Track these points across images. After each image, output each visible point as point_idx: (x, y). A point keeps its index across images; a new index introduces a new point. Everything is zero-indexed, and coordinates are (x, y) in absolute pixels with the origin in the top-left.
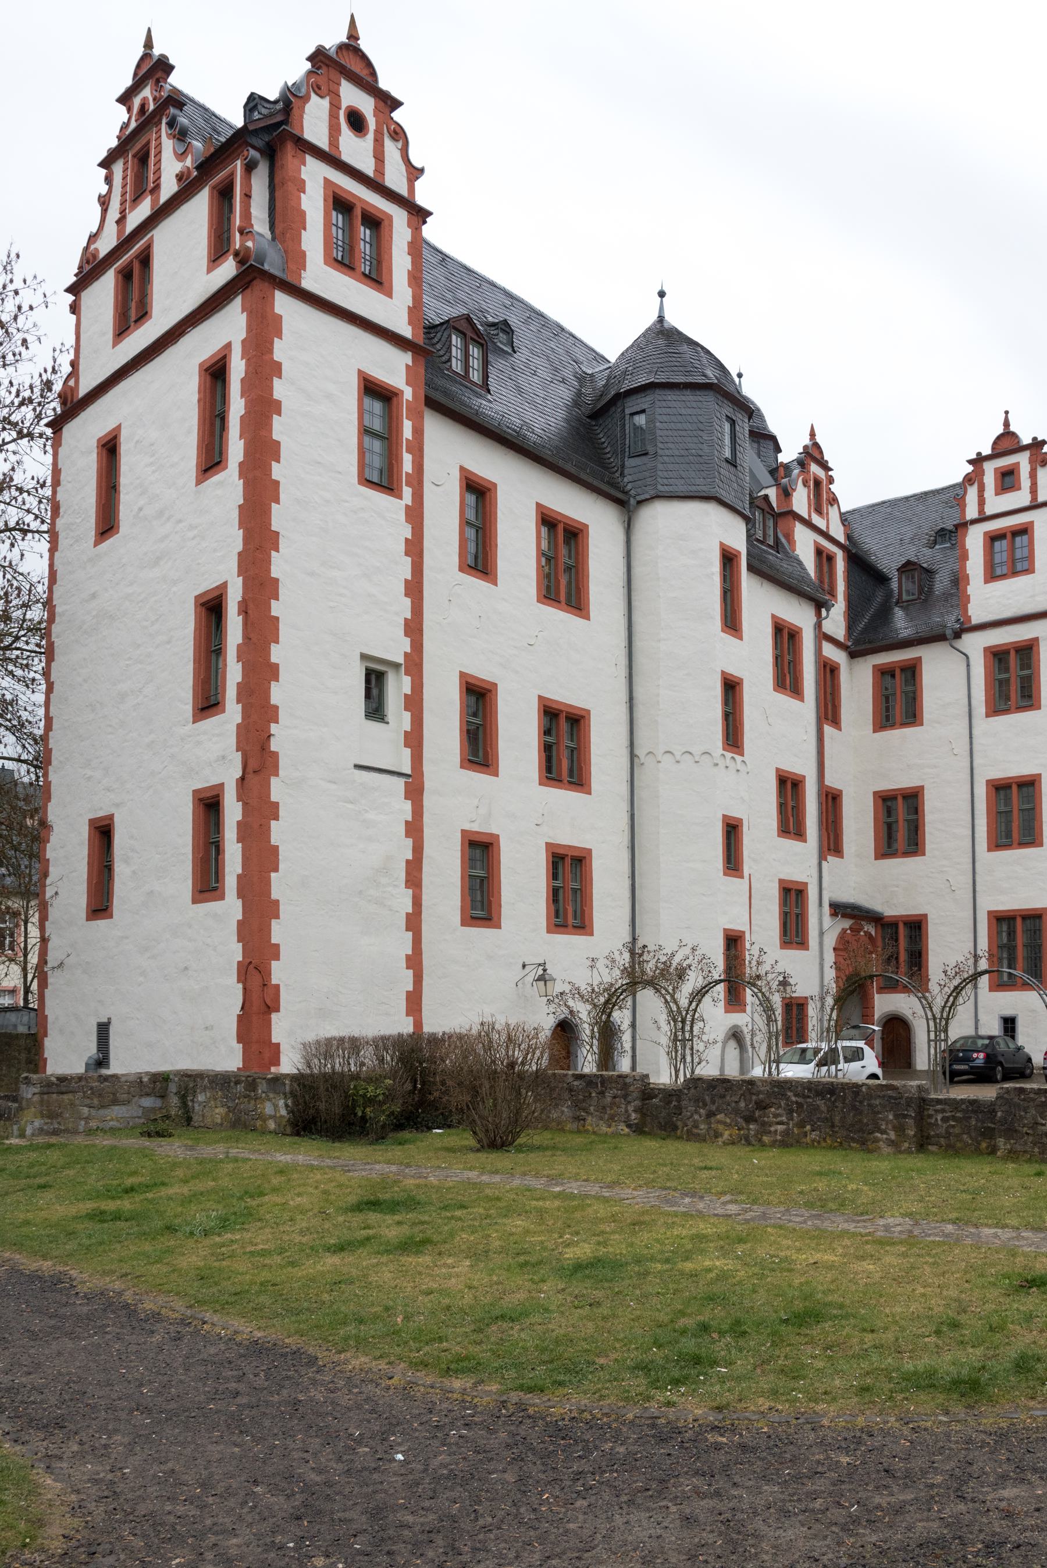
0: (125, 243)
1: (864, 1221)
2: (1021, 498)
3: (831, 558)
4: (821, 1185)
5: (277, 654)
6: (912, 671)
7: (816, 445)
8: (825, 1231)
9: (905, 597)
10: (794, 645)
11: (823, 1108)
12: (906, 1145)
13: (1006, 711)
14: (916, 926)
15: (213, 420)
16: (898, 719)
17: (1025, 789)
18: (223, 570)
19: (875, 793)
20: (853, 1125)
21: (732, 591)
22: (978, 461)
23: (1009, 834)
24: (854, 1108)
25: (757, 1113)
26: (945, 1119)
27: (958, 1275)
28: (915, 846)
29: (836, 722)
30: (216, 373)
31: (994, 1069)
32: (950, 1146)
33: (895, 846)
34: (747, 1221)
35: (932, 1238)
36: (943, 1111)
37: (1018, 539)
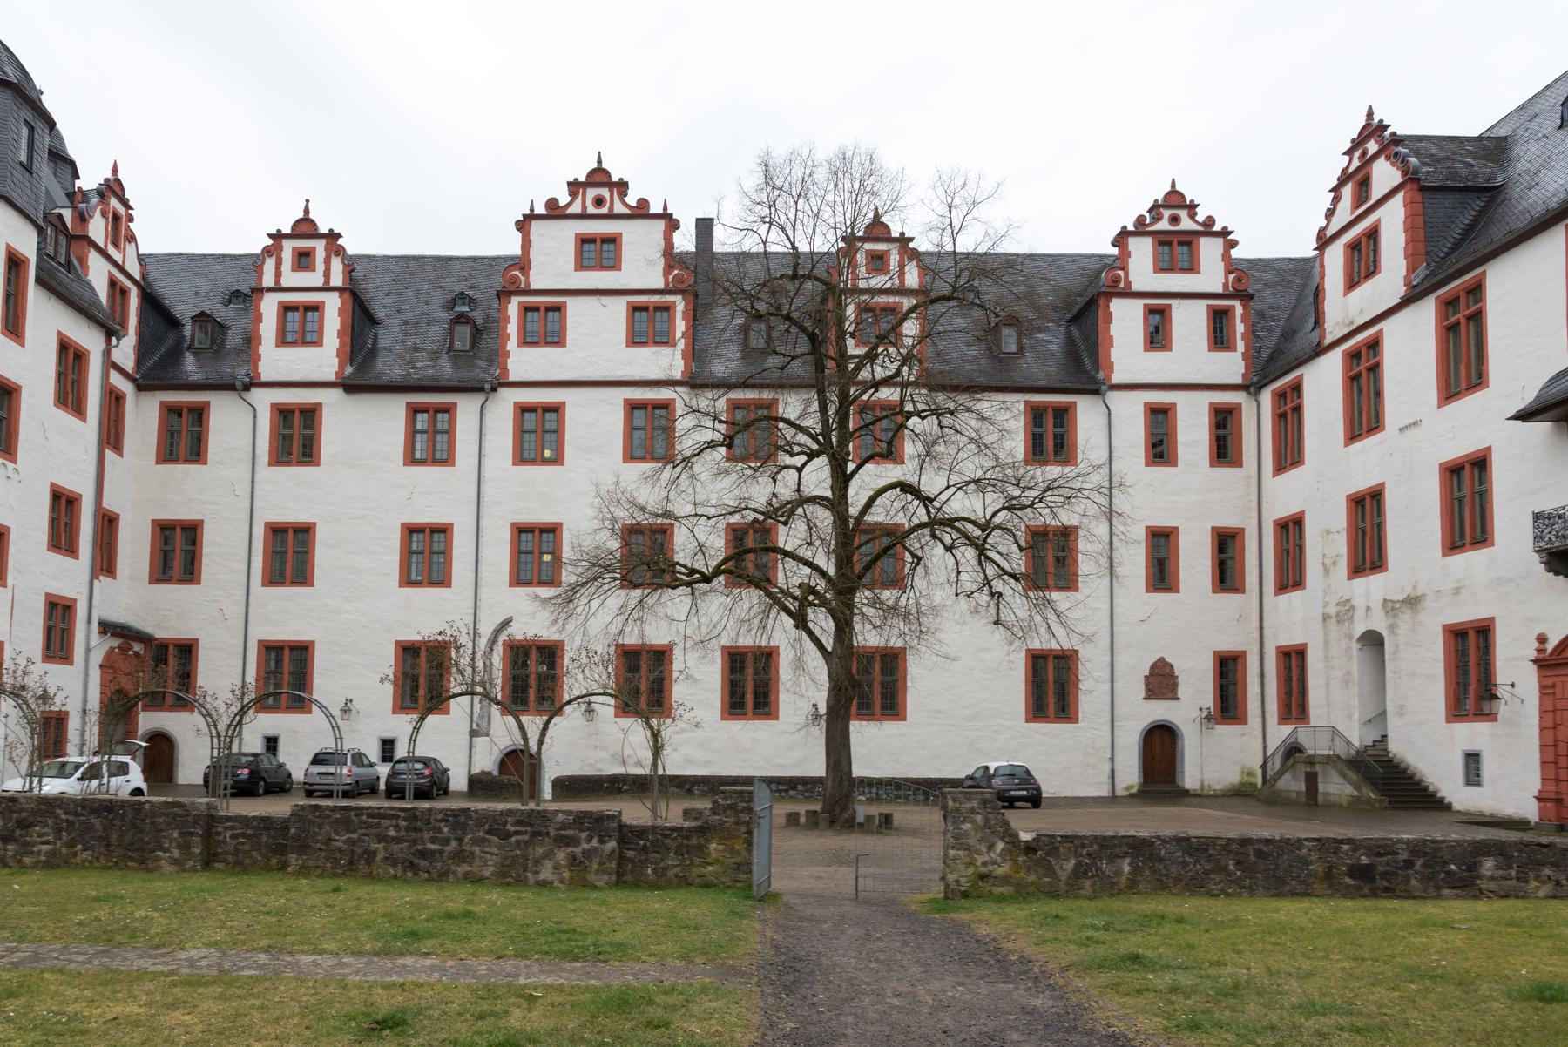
1: (163, 955)
2: (315, 279)
3: (124, 292)
4: (102, 912)
6: (199, 414)
7: (118, 181)
8: (117, 972)
9: (197, 345)
10: (80, 366)
11: (98, 826)
12: (191, 863)
13: (288, 463)
14: (187, 650)
16: (182, 454)
17: (300, 535)
19: (154, 521)
20: (131, 844)
21: (16, 296)
22: (278, 237)
23: (282, 573)
24: (134, 826)
25: (18, 833)
26: (234, 837)
27: (296, 1021)
29: (118, 448)
31: (256, 784)
32: (238, 863)
33: (171, 573)
34: (15, 966)
35: (246, 973)
36: (233, 828)
37: (309, 314)
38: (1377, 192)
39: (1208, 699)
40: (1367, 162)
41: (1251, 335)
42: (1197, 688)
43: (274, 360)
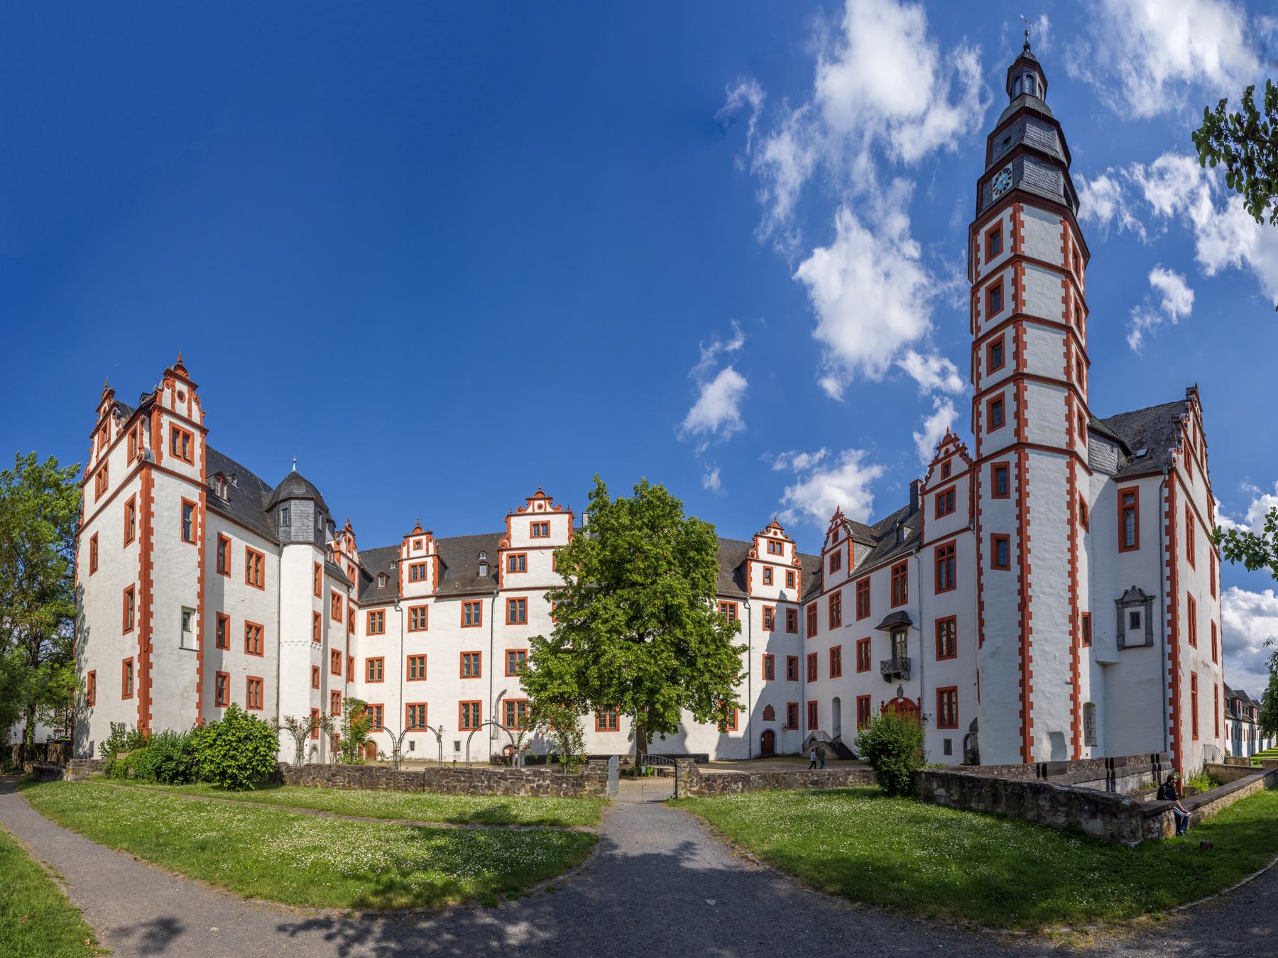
0: (99, 464)
2: (423, 552)
5: (152, 608)
6: (381, 614)
14: (380, 708)
15: (130, 522)
18: (133, 578)
28: (381, 678)
30: (131, 505)
38: (840, 539)
39: (785, 721)
40: (837, 526)
41: (803, 581)
42: (781, 717)
43: (409, 589)
